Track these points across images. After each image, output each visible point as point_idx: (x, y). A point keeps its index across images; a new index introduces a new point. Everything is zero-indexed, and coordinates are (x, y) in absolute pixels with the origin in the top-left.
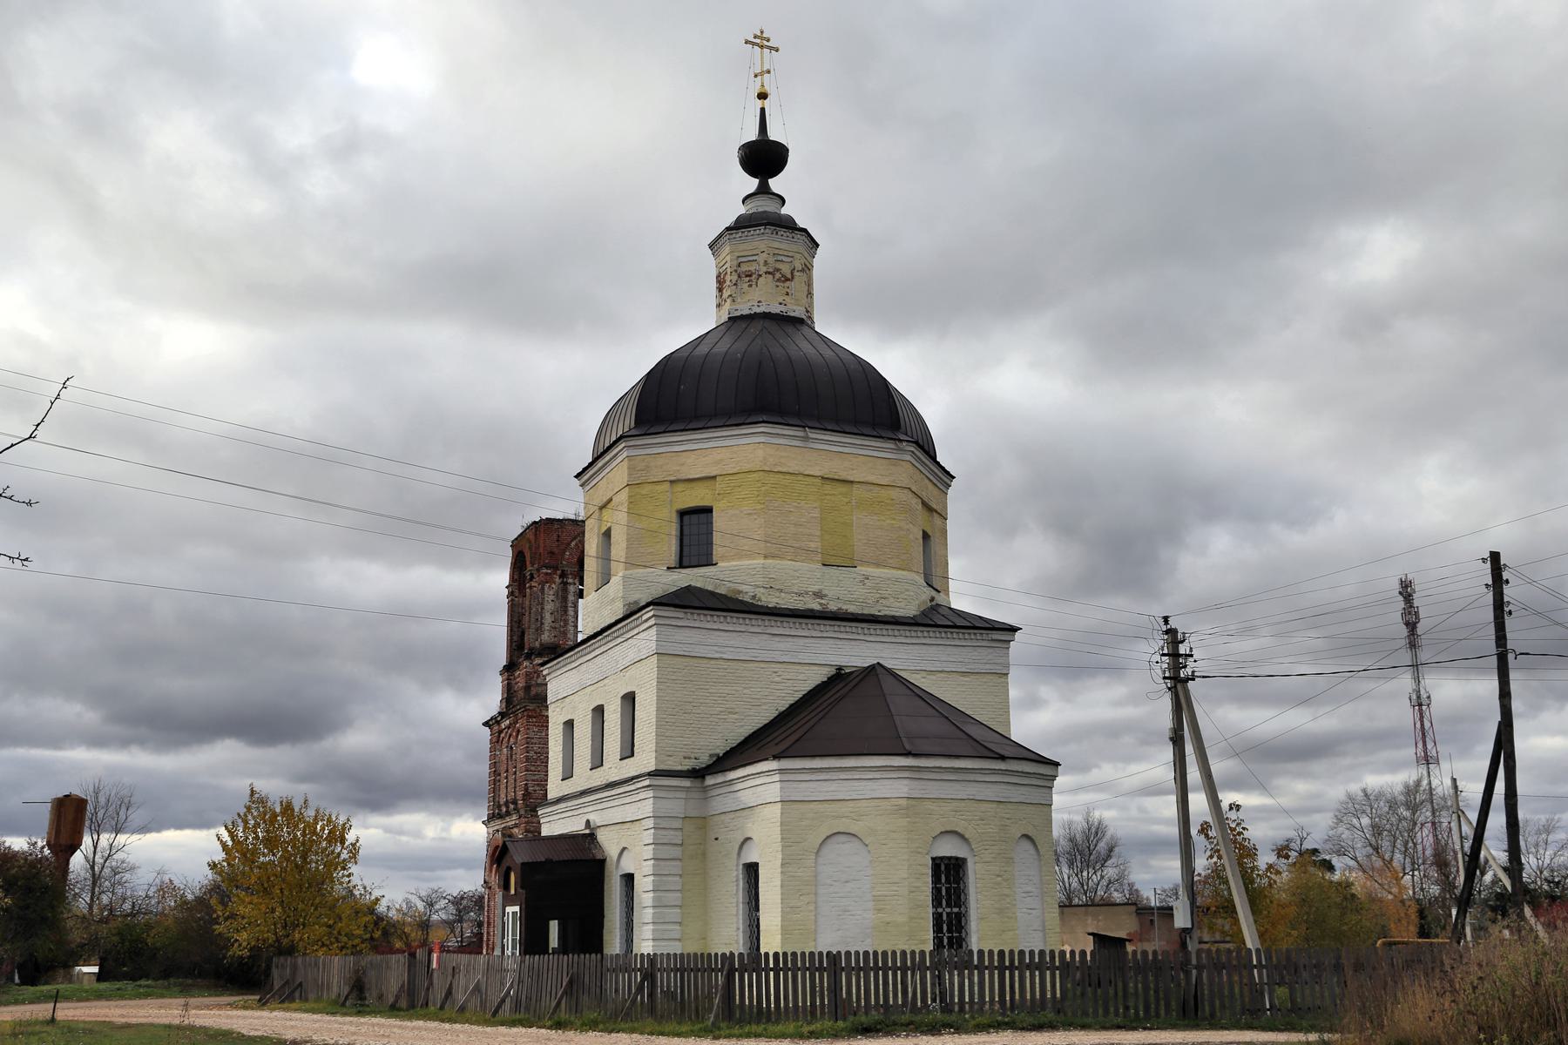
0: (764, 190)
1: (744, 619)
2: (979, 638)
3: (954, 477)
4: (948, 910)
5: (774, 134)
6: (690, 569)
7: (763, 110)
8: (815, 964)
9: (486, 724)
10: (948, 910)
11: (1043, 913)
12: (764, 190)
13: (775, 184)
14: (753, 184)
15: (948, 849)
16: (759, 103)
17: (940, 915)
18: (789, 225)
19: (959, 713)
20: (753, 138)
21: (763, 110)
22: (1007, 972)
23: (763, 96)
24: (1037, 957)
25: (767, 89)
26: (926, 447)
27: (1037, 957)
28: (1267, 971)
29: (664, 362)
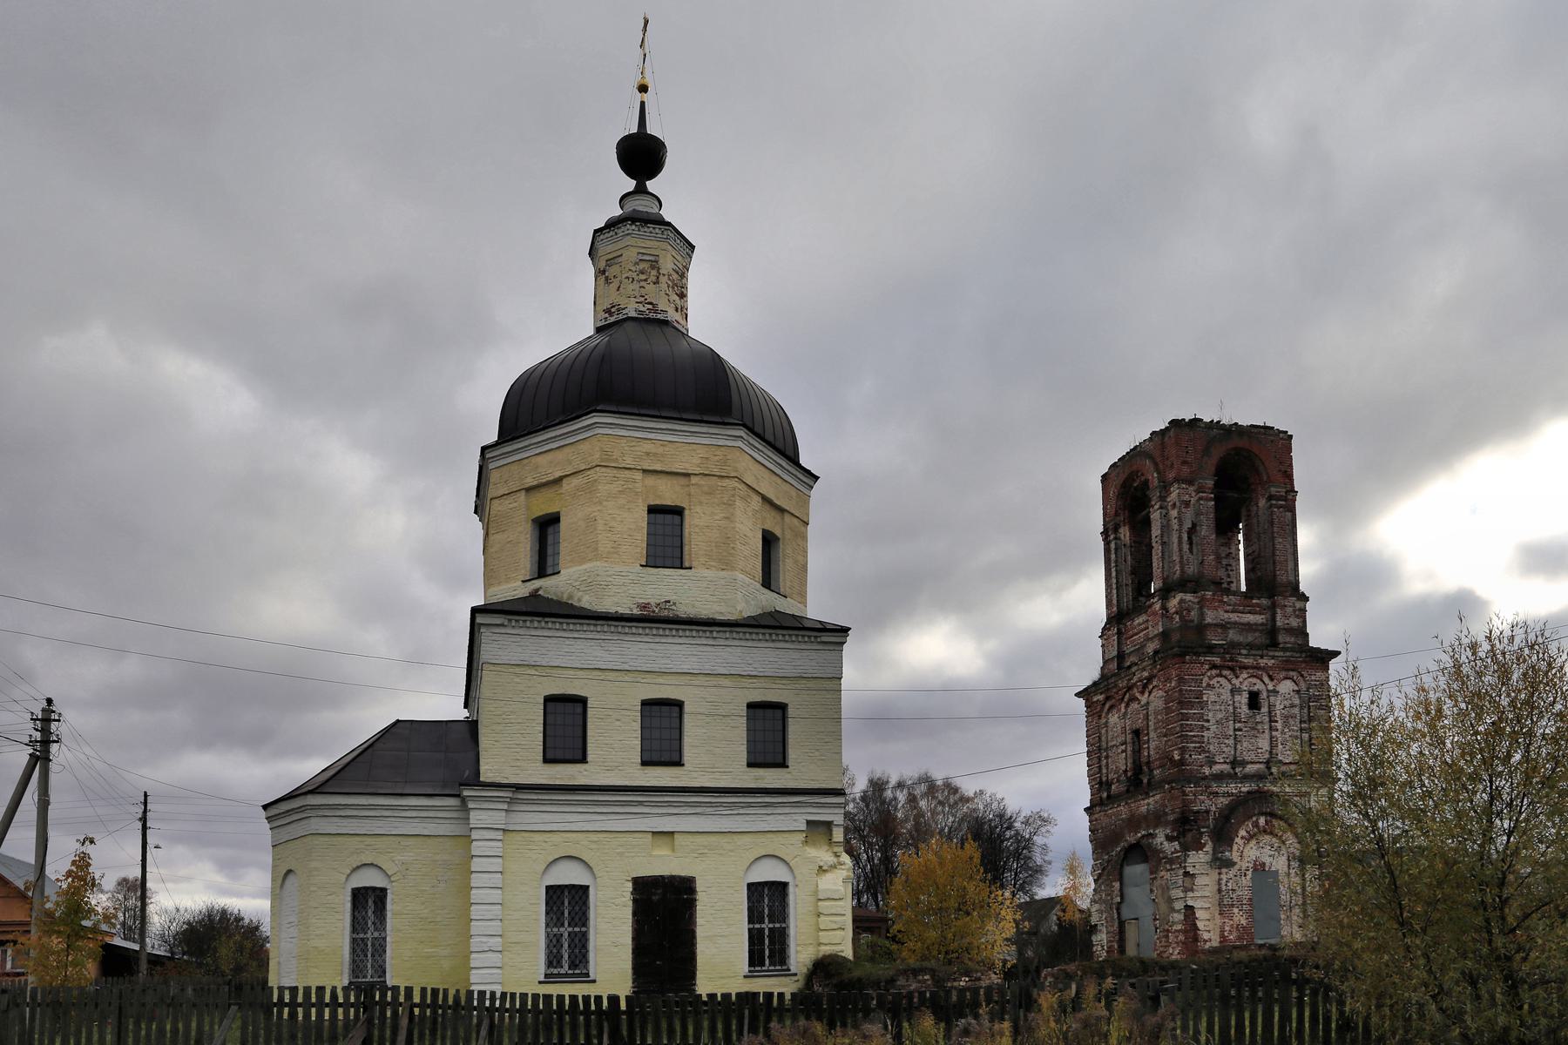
0: (641, 190)
1: (677, 630)
2: (800, 640)
3: (817, 478)
4: (570, 929)
5: (652, 129)
6: (671, 570)
7: (643, 104)
8: (438, 1001)
9: (1078, 695)
10: (570, 929)
11: (1289, 869)
12: (641, 190)
13: (651, 185)
14: (631, 184)
15: (569, 875)
16: (639, 96)
17: (559, 937)
18: (661, 222)
19: (580, 733)
20: (634, 130)
21: (643, 104)
22: (429, 1001)
23: (643, 89)
24: (313, 996)
25: (649, 81)
26: (782, 445)
27: (313, 996)
28: (392, 993)
29: (531, 370)
